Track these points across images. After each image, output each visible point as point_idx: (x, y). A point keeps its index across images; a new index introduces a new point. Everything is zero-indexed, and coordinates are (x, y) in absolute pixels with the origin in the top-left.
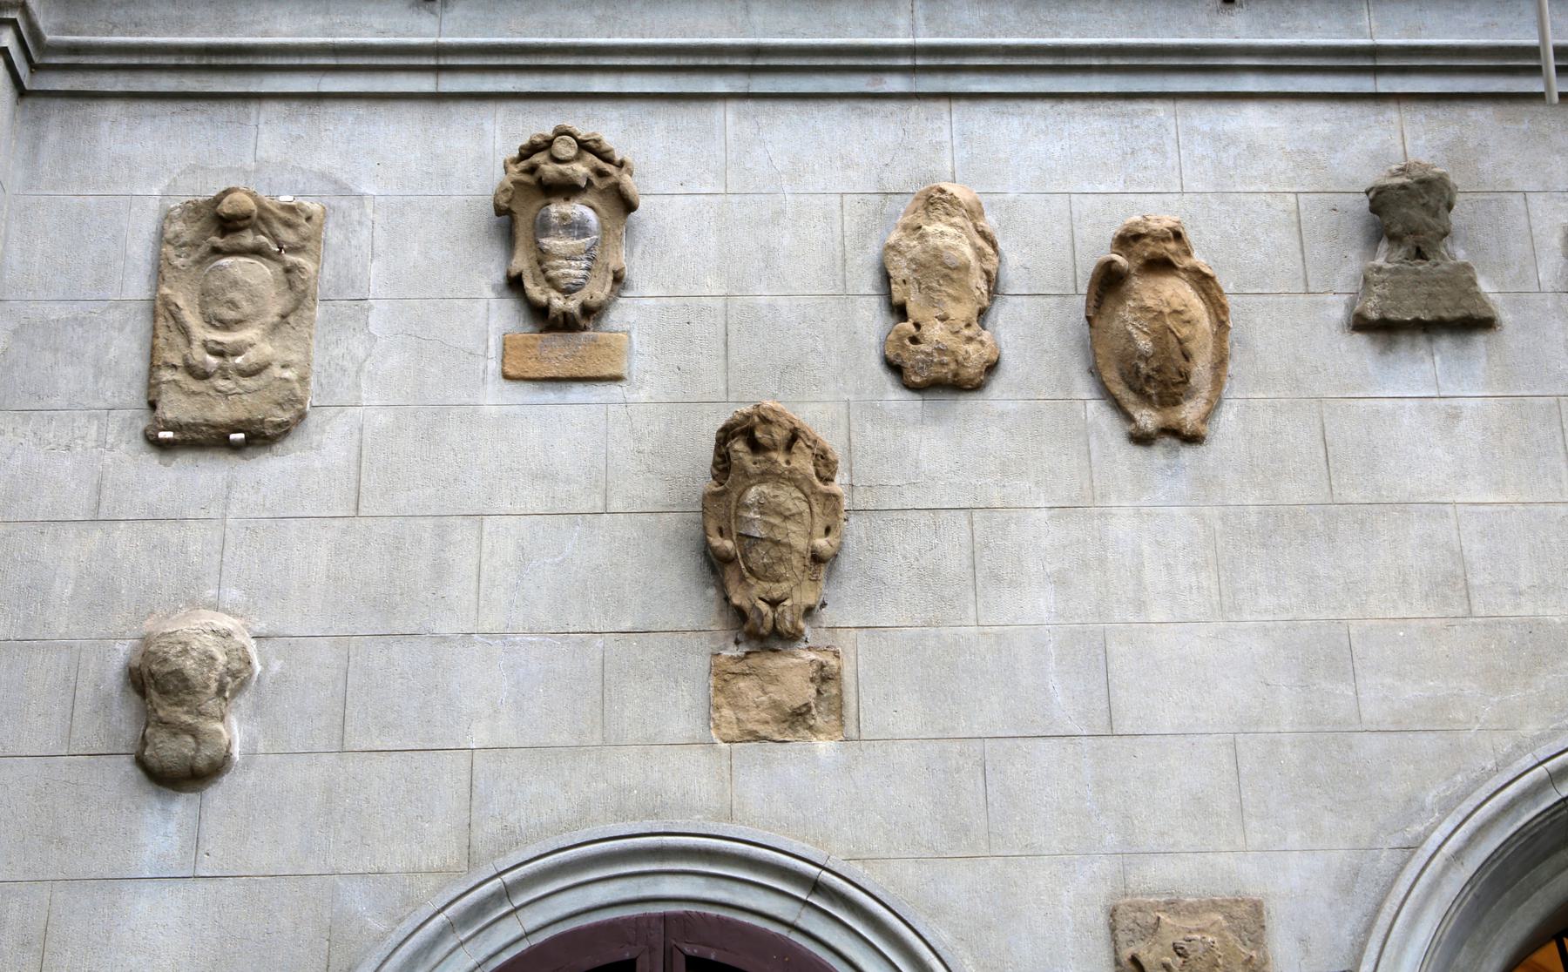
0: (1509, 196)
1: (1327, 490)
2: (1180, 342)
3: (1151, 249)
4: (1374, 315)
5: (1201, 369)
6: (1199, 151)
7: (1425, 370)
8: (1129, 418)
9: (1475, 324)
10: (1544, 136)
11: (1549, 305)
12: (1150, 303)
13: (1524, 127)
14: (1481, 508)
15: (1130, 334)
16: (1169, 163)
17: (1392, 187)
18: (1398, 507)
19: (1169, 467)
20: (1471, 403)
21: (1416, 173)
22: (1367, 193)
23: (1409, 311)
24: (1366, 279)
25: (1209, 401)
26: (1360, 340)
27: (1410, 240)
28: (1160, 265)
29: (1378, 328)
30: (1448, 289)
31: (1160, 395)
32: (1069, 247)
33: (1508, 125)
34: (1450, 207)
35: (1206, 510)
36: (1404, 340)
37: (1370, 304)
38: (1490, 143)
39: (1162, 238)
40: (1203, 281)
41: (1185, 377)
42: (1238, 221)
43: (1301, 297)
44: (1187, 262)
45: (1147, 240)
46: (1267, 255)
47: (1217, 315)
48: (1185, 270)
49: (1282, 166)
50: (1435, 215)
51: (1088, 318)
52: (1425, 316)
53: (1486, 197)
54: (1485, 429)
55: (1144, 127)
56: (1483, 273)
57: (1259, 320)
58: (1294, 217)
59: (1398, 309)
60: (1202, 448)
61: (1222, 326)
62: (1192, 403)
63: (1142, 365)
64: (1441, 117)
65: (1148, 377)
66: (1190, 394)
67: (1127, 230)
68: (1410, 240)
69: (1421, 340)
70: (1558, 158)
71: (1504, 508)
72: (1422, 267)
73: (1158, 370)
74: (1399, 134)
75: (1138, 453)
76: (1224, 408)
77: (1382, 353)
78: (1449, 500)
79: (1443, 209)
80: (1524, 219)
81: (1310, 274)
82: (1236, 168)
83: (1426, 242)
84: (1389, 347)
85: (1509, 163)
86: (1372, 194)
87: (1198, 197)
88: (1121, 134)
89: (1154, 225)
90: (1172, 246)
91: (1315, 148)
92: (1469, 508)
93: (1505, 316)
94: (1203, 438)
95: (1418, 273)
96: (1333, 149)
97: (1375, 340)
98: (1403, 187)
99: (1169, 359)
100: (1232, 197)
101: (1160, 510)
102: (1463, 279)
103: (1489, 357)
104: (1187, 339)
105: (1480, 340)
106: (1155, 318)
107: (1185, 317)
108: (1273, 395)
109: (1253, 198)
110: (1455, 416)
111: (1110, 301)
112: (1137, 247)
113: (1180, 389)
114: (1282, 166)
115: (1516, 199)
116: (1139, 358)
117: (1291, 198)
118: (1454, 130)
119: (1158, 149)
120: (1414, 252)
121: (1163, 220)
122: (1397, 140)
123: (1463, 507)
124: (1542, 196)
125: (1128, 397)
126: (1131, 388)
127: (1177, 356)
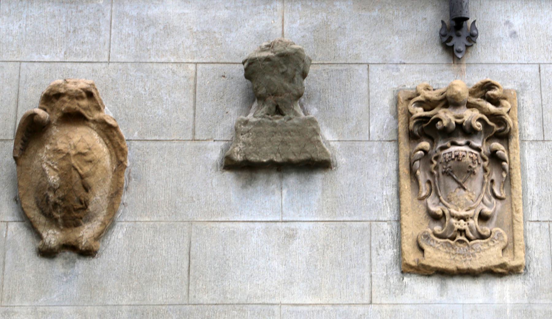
0: (356, 67)
1: (185, 293)
2: (82, 177)
3: (67, 105)
4: (239, 158)
5: (99, 198)
6: (126, 30)
7: (277, 201)
8: (39, 237)
9: (316, 165)
10: (389, 21)
11: (374, 151)
12: (61, 146)
13: (375, 13)
14: (300, 308)
15: (44, 170)
16: (101, 39)
17: (260, 59)
18: (238, 307)
19: (65, 274)
20: (305, 226)
21: (279, 49)
22: (243, 63)
23: (266, 154)
24: (236, 129)
25: (103, 223)
26: (229, 176)
27: (271, 100)
28: (74, 118)
29: (244, 168)
30: (297, 138)
31: (63, 218)
32: (14, 103)
33: (363, 13)
34: (304, 75)
35: (89, 309)
36: (262, 177)
37: (237, 149)
38: (348, 26)
39: (79, 97)
40: (108, 131)
41: (85, 205)
42: (149, 84)
43: (188, 143)
44: (97, 115)
45: (65, 98)
46: (167, 110)
47: (117, 157)
48: (94, 121)
49: (188, 42)
50: (292, 81)
51: (15, 158)
52: (278, 159)
53: (339, 67)
54: (313, 246)
55: (86, 12)
56: (328, 125)
57: (153, 161)
58: (192, 82)
59: (257, 153)
60: (94, 260)
61: (120, 165)
62: (90, 225)
63: (51, 195)
64: (314, 6)
65: (55, 205)
66: (89, 218)
67: (51, 90)
68: (271, 100)
69: (275, 177)
70: (396, 38)
71: (318, 308)
72: (279, 120)
73: (63, 199)
74: (280, 19)
75: (43, 264)
76: (116, 229)
77: (244, 187)
78: (277, 301)
79: (298, 77)
80: (365, 85)
81: (198, 125)
82: (153, 43)
83: (283, 102)
84: (250, 182)
85: (360, 41)
86: (246, 64)
87: (120, 66)
88: (67, 17)
89: (71, 87)
90: (84, 103)
91: (215, 29)
92: (291, 308)
93: (341, 159)
94: (96, 252)
95: (275, 125)
96: (228, 30)
97: (239, 177)
98: (268, 59)
99: (72, 190)
100: (146, 66)
101: (52, 309)
102: (309, 131)
103: (323, 190)
104: (87, 175)
105: (319, 177)
106: (63, 159)
107: (88, 158)
108: (155, 218)
109: (163, 67)
110: (291, 236)
111: (34, 146)
112: (58, 103)
113: (81, 214)
114: (188, 42)
115: (361, 70)
116: (49, 189)
117: (192, 67)
118: (321, 16)
119: (95, 29)
120: (274, 109)
121: (80, 81)
122: (278, 23)
123: (286, 307)
124: (381, 67)
125: (40, 219)
126: (43, 213)
127: (78, 188)
